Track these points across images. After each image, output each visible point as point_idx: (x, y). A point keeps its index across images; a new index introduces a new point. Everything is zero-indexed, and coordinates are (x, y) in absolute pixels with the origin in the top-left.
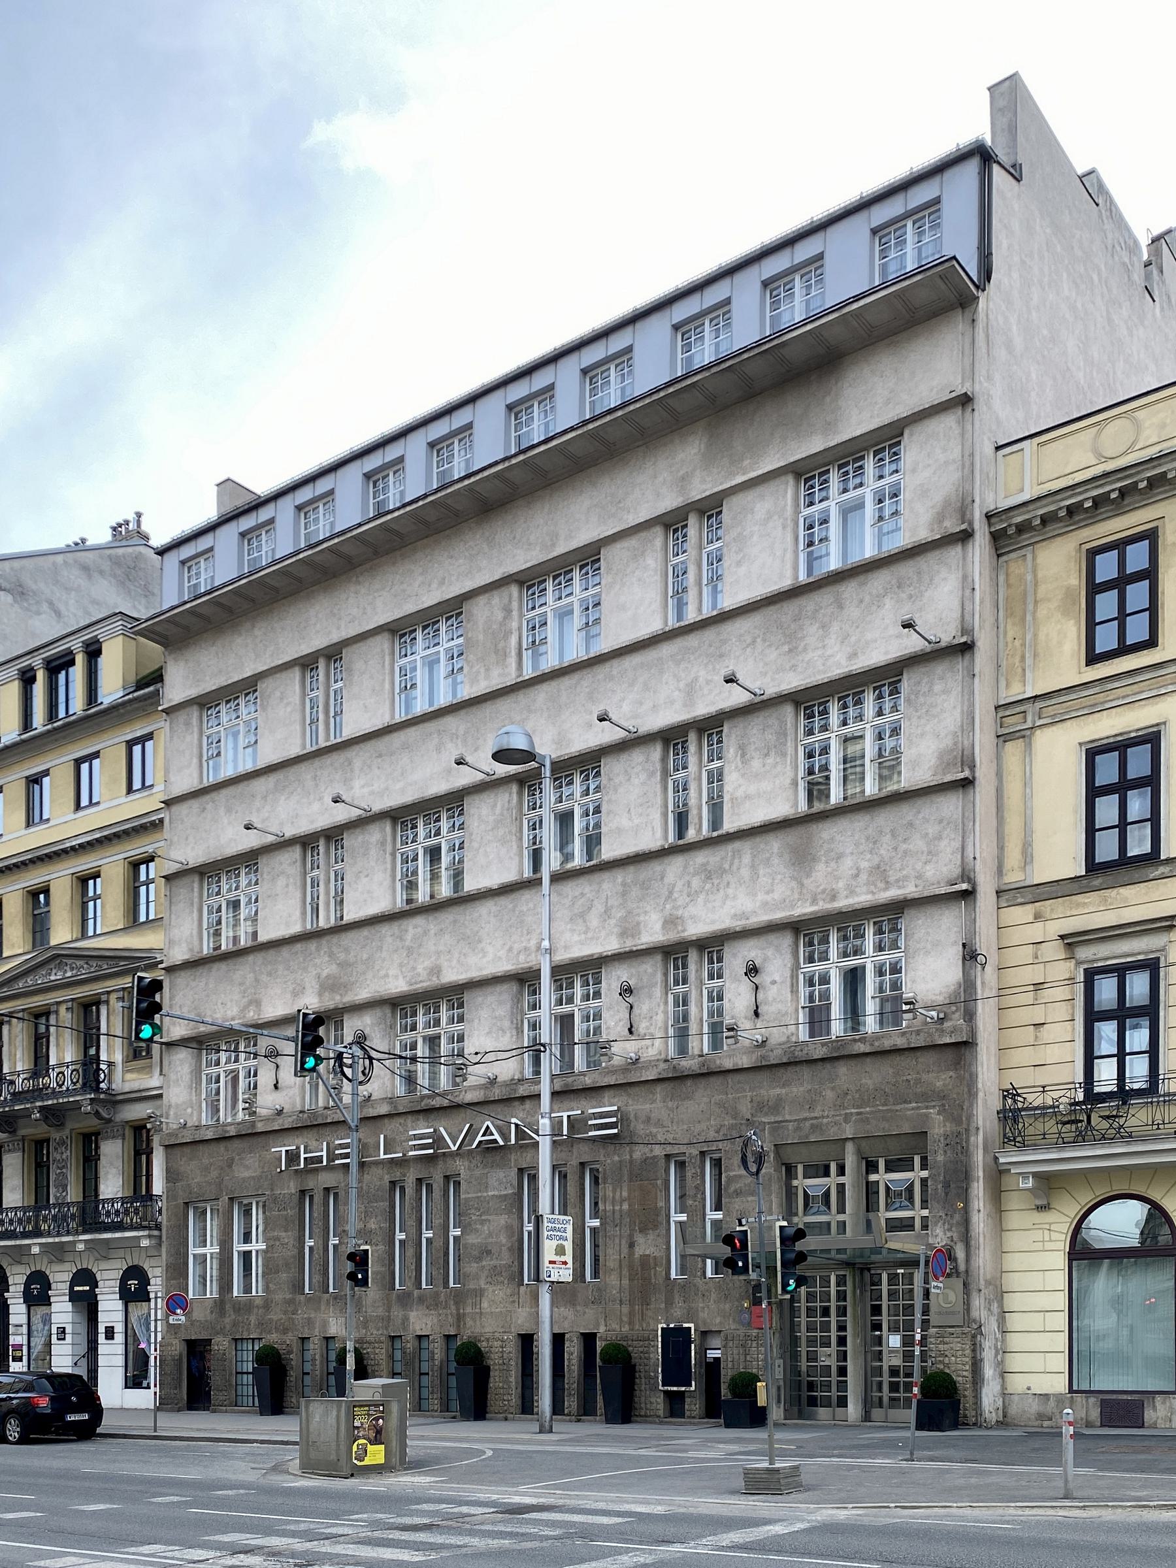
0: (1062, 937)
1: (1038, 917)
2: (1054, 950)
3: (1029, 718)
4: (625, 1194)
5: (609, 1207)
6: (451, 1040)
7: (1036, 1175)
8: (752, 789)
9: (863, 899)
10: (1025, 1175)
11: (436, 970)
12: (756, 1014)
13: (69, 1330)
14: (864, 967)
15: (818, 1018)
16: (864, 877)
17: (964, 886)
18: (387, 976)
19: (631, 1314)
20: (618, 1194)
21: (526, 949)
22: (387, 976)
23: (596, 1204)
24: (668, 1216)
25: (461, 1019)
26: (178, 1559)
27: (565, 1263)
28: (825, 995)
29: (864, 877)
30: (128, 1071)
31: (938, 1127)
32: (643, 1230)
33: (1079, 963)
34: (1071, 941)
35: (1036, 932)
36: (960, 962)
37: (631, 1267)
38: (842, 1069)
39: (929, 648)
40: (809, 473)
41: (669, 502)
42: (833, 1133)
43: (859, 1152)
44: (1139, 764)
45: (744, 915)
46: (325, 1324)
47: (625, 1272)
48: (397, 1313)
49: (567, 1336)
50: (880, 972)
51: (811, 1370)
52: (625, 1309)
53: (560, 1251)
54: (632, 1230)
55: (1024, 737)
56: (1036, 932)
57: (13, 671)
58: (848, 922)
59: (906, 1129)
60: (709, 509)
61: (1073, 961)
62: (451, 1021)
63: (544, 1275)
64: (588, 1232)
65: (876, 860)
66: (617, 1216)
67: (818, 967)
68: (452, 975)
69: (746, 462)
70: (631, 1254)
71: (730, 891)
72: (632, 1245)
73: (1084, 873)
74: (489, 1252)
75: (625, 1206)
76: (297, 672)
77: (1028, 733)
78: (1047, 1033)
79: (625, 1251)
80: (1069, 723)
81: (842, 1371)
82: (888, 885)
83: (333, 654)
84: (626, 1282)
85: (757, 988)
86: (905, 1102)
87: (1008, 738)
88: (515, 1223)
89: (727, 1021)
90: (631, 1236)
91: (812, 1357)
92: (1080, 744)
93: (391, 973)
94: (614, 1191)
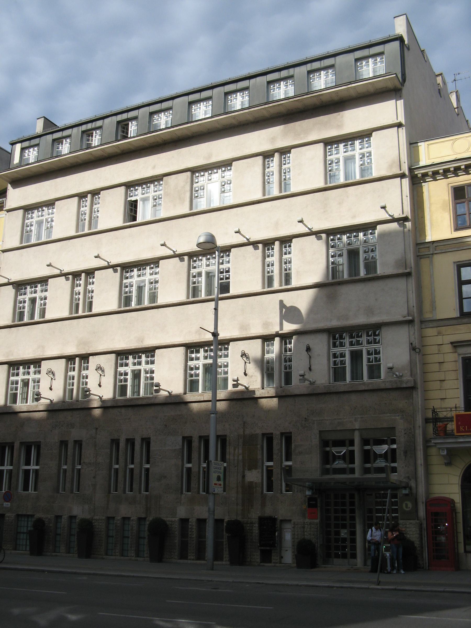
0: (452, 343)
1: (439, 334)
2: (448, 348)
3: (431, 250)
4: (240, 451)
5: (232, 458)
6: (146, 372)
7: (447, 449)
9: (361, 320)
10: (443, 449)
12: (310, 369)
14: (362, 351)
15: (338, 373)
17: (410, 318)
20: (237, 451)
23: (67, 458)
24: (263, 463)
25: (153, 362)
27: (220, 485)
28: (343, 363)
31: (401, 425)
32: (250, 469)
33: (459, 355)
34: (456, 345)
35: (439, 340)
36: (409, 351)
38: (353, 397)
39: (390, 218)
40: (329, 143)
41: (267, 147)
42: (349, 426)
43: (361, 435)
49: (190, 520)
50: (369, 353)
51: (337, 541)
53: (219, 478)
55: (429, 257)
56: (439, 340)
58: (354, 331)
59: (385, 425)
60: (284, 152)
61: (456, 354)
62: (35, 373)
63: (211, 491)
64: (62, 471)
67: (338, 350)
68: (149, 342)
69: (302, 136)
72: (244, 477)
73: (459, 316)
74: (165, 477)
75: (241, 457)
76: (76, 199)
77: (431, 256)
78: (447, 384)
80: (448, 254)
81: (353, 541)
83: (95, 193)
85: (310, 357)
86: (384, 413)
87: (422, 257)
88: (180, 463)
89: (155, 381)
90: (244, 472)
92: (454, 262)
94: (235, 450)
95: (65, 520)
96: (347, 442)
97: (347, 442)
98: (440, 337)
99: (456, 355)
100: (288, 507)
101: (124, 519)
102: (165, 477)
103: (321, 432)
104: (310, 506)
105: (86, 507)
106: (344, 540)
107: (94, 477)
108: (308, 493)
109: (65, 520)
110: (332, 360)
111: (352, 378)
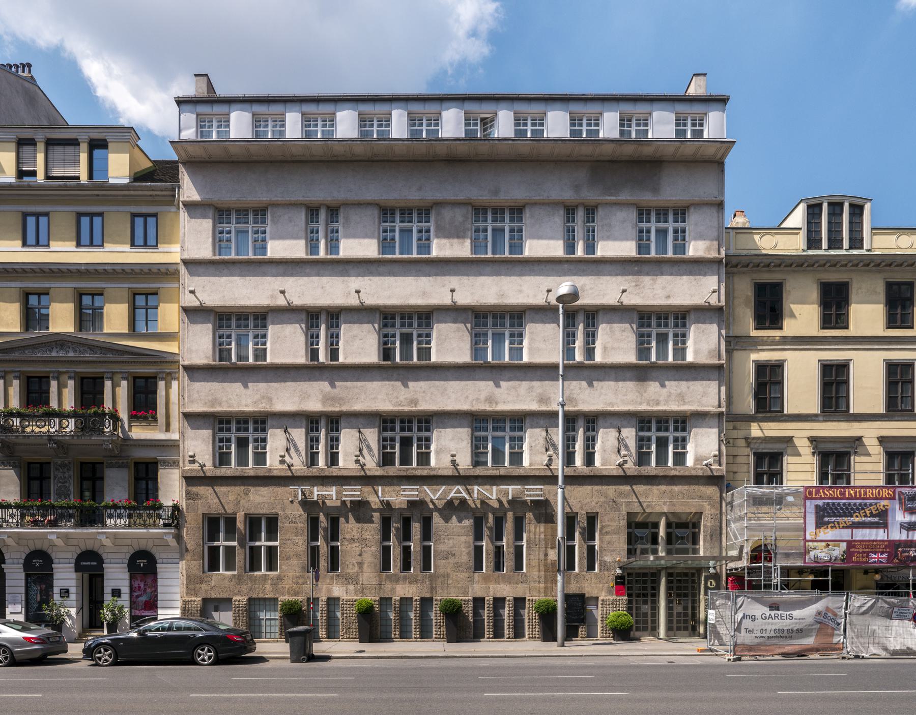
1: (735, 428)
8: (616, 345)
11: (415, 402)
13: (73, 590)
16: (673, 397)
18: (376, 398)
19: (546, 588)
21: (478, 399)
22: (376, 398)
26: (746, 673)
29: (673, 397)
30: (837, 406)
37: (545, 566)
44: (141, 383)
45: (611, 404)
46: (329, 590)
47: (542, 568)
48: (388, 586)
52: (542, 586)
54: (546, 548)
57: (13, 135)
65: (679, 391)
66: (537, 540)
70: (546, 560)
71: (603, 391)
72: (546, 555)
74: (454, 555)
75: (542, 536)
79: (542, 557)
82: (685, 403)
84: (542, 573)
91: (685, 608)
93: (380, 397)
94: (535, 528)
95: (322, 604)
96: (691, 525)
97: (691, 525)
98: (736, 431)
99: (749, 449)
100: (599, 587)
101: (402, 599)
102: (454, 555)
103: (628, 514)
104: (617, 583)
105: (351, 587)
106: (645, 615)
107: (360, 555)
108: (619, 571)
109: (322, 604)
110: (217, 444)
111: (657, 463)
